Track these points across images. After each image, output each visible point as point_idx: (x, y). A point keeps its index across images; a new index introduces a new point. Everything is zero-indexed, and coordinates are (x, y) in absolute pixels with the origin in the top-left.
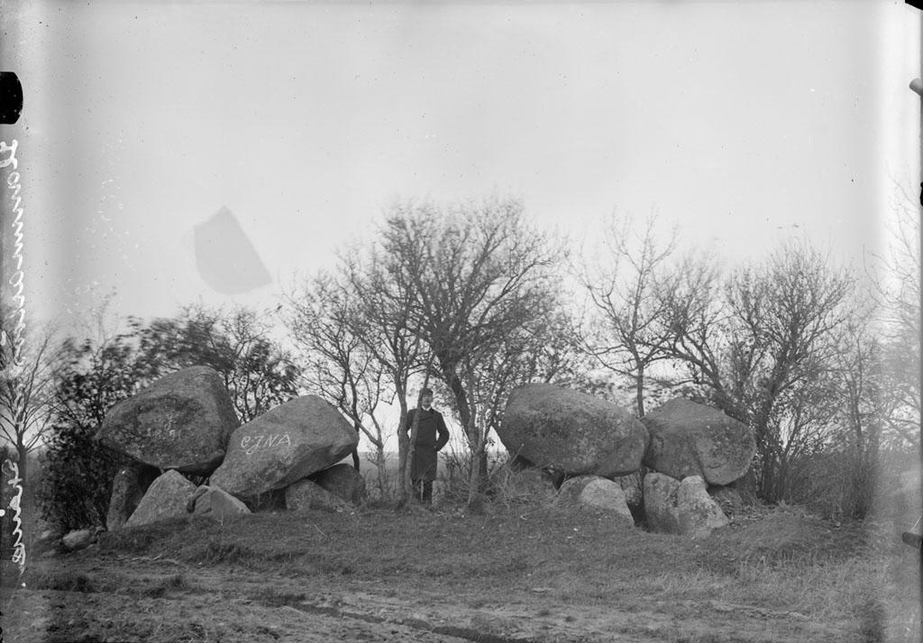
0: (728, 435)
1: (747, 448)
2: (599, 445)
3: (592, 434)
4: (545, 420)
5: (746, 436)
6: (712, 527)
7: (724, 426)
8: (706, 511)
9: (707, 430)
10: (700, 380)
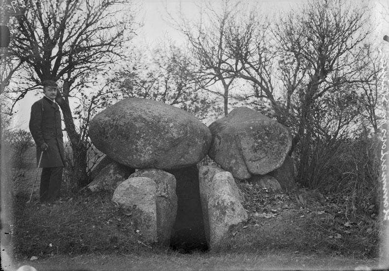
0: (267, 134)
1: (283, 144)
2: (155, 144)
3: (146, 136)
5: (282, 134)
6: (230, 224)
7: (264, 127)
8: (226, 208)
10: (260, 95)
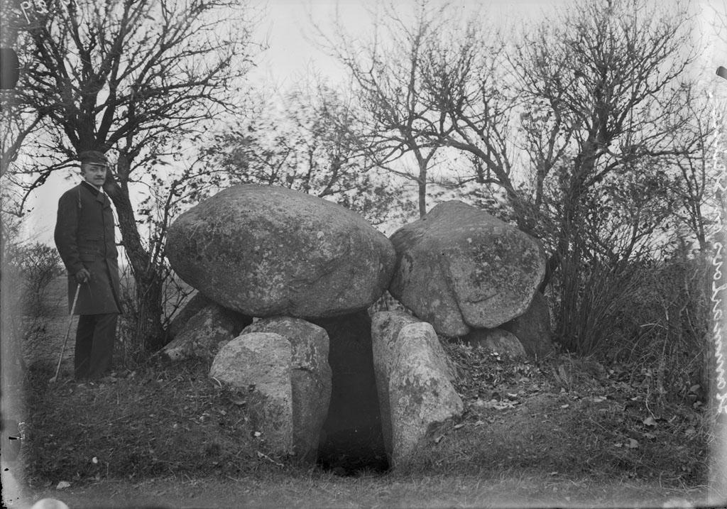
0: (500, 251)
1: (528, 270)
2: (289, 271)
3: (273, 255)
4: (210, 234)
5: (527, 252)
6: (430, 420)
7: (493, 239)
8: (422, 390)
9: (467, 245)
